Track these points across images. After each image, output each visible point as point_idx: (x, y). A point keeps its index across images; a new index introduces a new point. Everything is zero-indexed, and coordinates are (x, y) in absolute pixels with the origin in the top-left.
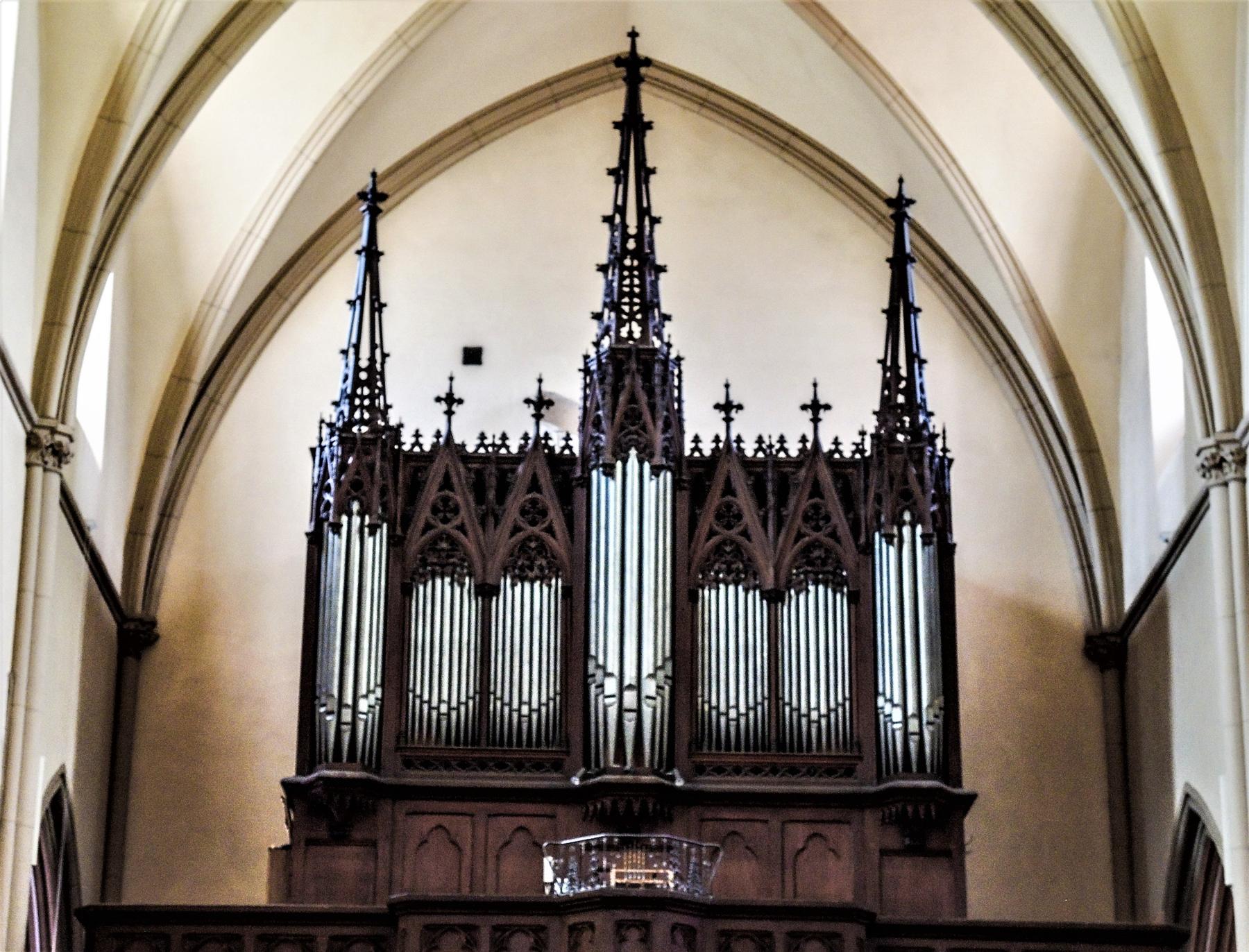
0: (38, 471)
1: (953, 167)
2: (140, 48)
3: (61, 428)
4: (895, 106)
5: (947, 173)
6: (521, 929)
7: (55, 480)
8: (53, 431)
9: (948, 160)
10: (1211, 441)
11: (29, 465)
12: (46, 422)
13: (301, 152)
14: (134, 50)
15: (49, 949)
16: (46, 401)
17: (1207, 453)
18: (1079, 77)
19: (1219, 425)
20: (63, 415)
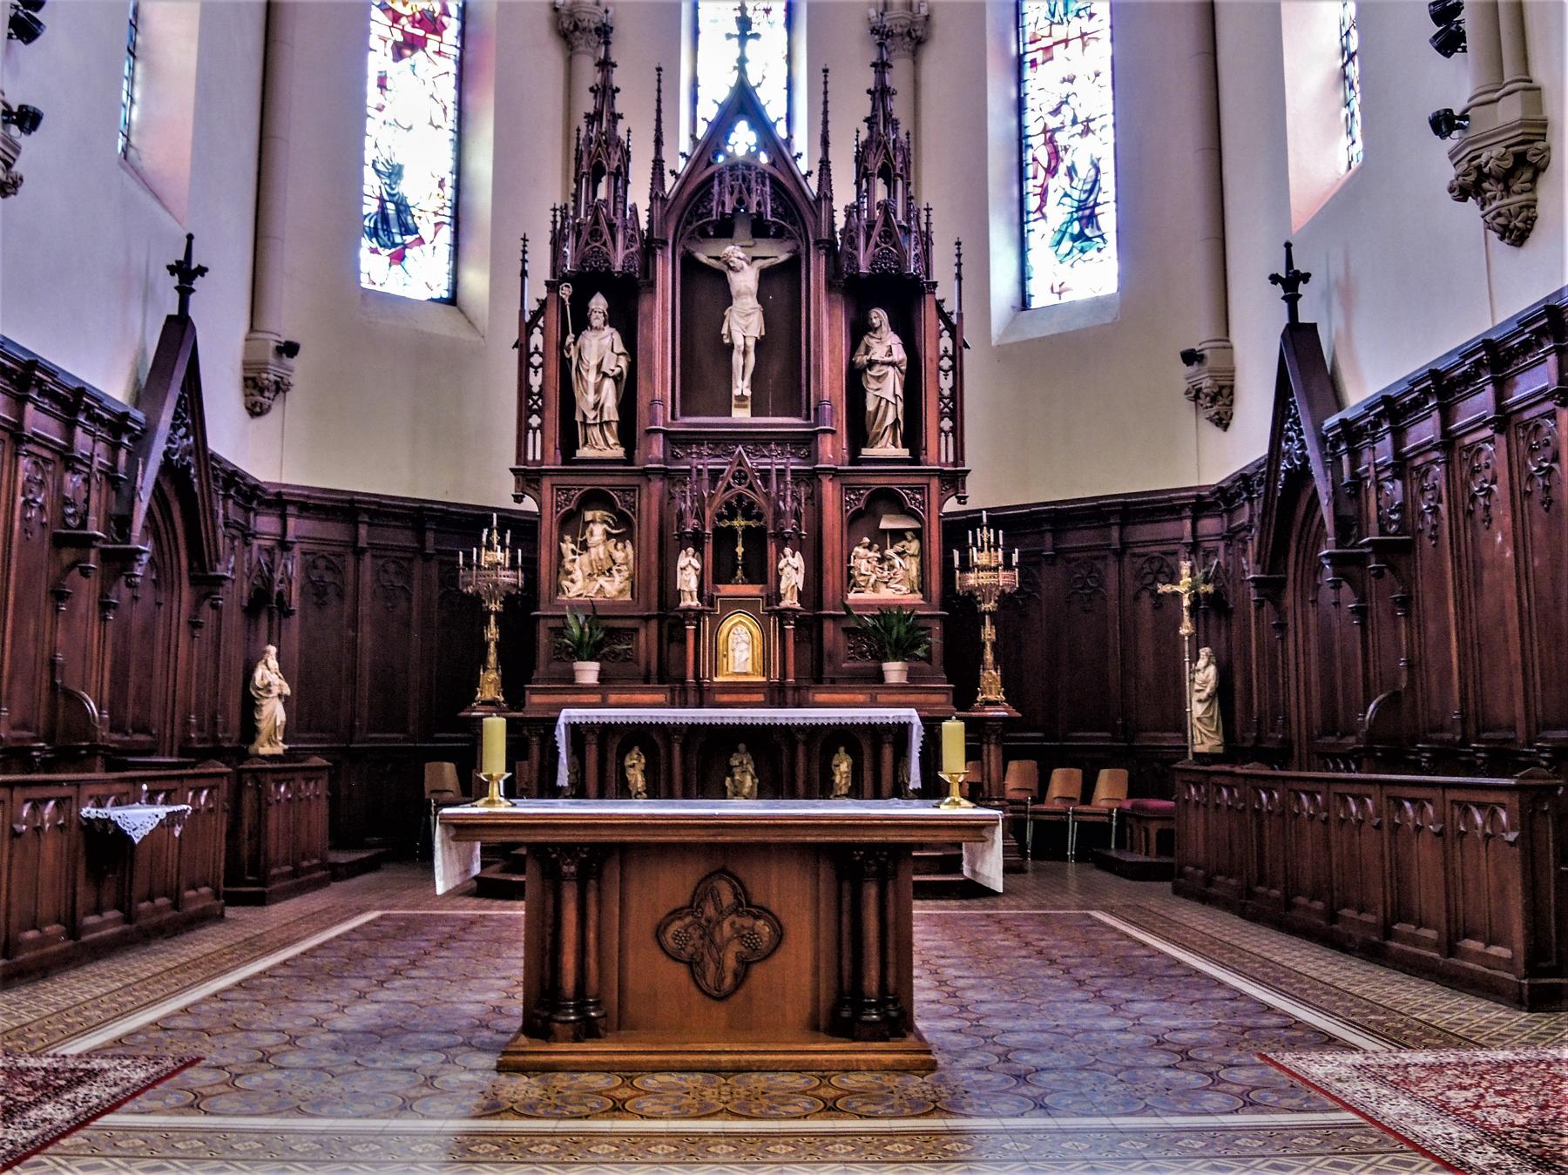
6: (739, 691)
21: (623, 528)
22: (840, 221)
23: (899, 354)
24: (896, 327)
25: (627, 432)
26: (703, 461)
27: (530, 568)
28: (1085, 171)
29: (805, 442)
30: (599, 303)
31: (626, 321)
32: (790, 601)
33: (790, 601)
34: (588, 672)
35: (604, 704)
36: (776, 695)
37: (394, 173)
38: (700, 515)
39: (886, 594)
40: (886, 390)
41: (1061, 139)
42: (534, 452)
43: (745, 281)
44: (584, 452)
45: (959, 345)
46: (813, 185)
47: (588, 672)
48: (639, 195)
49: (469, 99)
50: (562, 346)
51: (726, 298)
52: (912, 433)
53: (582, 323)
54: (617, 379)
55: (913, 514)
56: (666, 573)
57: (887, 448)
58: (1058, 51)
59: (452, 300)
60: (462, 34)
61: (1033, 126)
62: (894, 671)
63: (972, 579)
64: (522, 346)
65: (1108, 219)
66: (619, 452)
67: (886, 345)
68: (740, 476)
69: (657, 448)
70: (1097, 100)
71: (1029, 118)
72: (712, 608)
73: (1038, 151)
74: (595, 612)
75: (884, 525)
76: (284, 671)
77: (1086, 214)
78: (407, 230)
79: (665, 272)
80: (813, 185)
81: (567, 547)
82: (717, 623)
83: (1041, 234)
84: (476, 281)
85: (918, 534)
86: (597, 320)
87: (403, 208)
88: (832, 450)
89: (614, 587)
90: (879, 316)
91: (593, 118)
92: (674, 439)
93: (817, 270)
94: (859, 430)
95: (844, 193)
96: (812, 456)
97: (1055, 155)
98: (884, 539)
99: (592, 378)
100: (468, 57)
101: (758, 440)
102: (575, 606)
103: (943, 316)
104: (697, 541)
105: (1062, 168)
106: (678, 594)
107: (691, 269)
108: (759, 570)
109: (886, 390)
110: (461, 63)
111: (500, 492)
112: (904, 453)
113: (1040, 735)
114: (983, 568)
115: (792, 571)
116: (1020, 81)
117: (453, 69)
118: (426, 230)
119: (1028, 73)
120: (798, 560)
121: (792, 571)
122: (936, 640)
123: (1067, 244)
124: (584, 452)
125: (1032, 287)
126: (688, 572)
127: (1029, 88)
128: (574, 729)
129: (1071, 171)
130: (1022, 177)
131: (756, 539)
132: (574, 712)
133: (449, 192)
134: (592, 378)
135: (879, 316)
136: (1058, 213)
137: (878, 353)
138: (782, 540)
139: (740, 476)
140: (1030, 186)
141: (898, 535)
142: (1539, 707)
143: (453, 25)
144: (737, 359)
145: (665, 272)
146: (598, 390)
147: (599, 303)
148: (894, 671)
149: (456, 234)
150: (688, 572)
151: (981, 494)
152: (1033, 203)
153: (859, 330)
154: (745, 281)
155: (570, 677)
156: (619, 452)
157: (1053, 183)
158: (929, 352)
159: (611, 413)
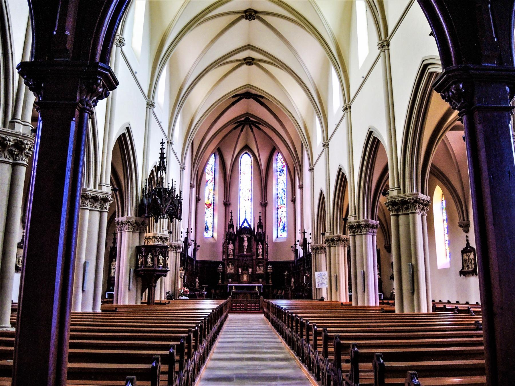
0: (169, 146)
1: (318, 10)
2: (166, 36)
3: (152, 101)
4: (296, 56)
5: (317, 11)
6: (245, 282)
7: (171, 147)
8: (171, 141)
9: (317, 8)
10: (345, 105)
11: (190, 188)
12: (150, 100)
13: (183, 5)
14: (164, 36)
15: (5, 1)
16: (150, 97)
17: (344, 107)
18: (329, 48)
19: (347, 102)
20: (153, 99)
21: (233, 265)
22: (256, 233)
23: (262, 247)
24: (261, 244)
25: (234, 255)
26: (242, 259)
27: (224, 269)
28: (284, 223)
29: (252, 257)
30: (231, 242)
31: (233, 243)
32: (250, 273)
33: (250, 273)
34: (230, 280)
35: (232, 284)
36: (249, 283)
37: (206, 223)
38: (241, 264)
39: (260, 272)
40: (260, 251)
41: (281, 218)
42: (224, 257)
43: (246, 239)
44: (229, 257)
45: (268, 246)
46: (253, 229)
47: (230, 280)
48: (235, 230)
49: (214, 213)
50: (227, 246)
51: (244, 241)
52: (263, 255)
53: (229, 244)
54: (233, 250)
55: (263, 264)
56: (238, 270)
57: (260, 257)
58: (281, 208)
59: (213, 237)
60: (214, 205)
61: (279, 216)
62: (260, 280)
63: (268, 271)
64: (223, 246)
65: (286, 228)
66: (233, 257)
67: (260, 246)
68: (245, 260)
69: (237, 257)
70: (285, 215)
71: (278, 215)
72: (243, 274)
73: (279, 219)
74: (231, 274)
75: (260, 265)
76: (198, 280)
77: (284, 227)
78: (208, 229)
79: (238, 238)
80: (253, 229)
81: (228, 267)
82: (243, 275)
83: (279, 229)
84: (215, 235)
85: (263, 266)
86: (231, 243)
87: (207, 227)
88: (254, 257)
89: (232, 271)
90: (260, 243)
91: (230, 222)
92: (238, 256)
93: (253, 238)
94: (258, 255)
95: (256, 230)
96: (253, 258)
97: (281, 220)
98: (260, 266)
99: (230, 250)
100: (214, 208)
101: (247, 256)
102: (229, 273)
103: (266, 243)
104: (241, 267)
105: (281, 222)
106: (239, 272)
107: (240, 237)
108: (247, 270)
109: (260, 251)
110: (213, 209)
111: (220, 259)
112: (262, 257)
113: (262, 291)
114: (269, 270)
115: (250, 270)
116: (277, 211)
117: (213, 210)
118: (210, 229)
119: (278, 210)
120: (251, 269)
121: (250, 270)
122: (265, 277)
123: (282, 231)
124: (229, 257)
125: (278, 235)
126: (240, 270)
127: (278, 212)
128: (229, 286)
129: (282, 222)
130: (277, 222)
131: (247, 267)
132: (229, 285)
133: (212, 224)
134: (230, 250)
135: (260, 243)
136: (281, 227)
137: (259, 247)
138: (249, 267)
139: (245, 260)
140: (278, 223)
141: (261, 266)
142: (189, 302)
143: (213, 204)
144: (245, 247)
145: (238, 238)
146: (231, 251)
147: (231, 242)
148: (260, 280)
149: (213, 229)
150: (240, 270)
151: (270, 260)
152: (278, 225)
153: (258, 244)
154: (246, 239)
155: (228, 281)
156: (233, 257)
157: (280, 223)
158: (265, 247)
159: (232, 253)
